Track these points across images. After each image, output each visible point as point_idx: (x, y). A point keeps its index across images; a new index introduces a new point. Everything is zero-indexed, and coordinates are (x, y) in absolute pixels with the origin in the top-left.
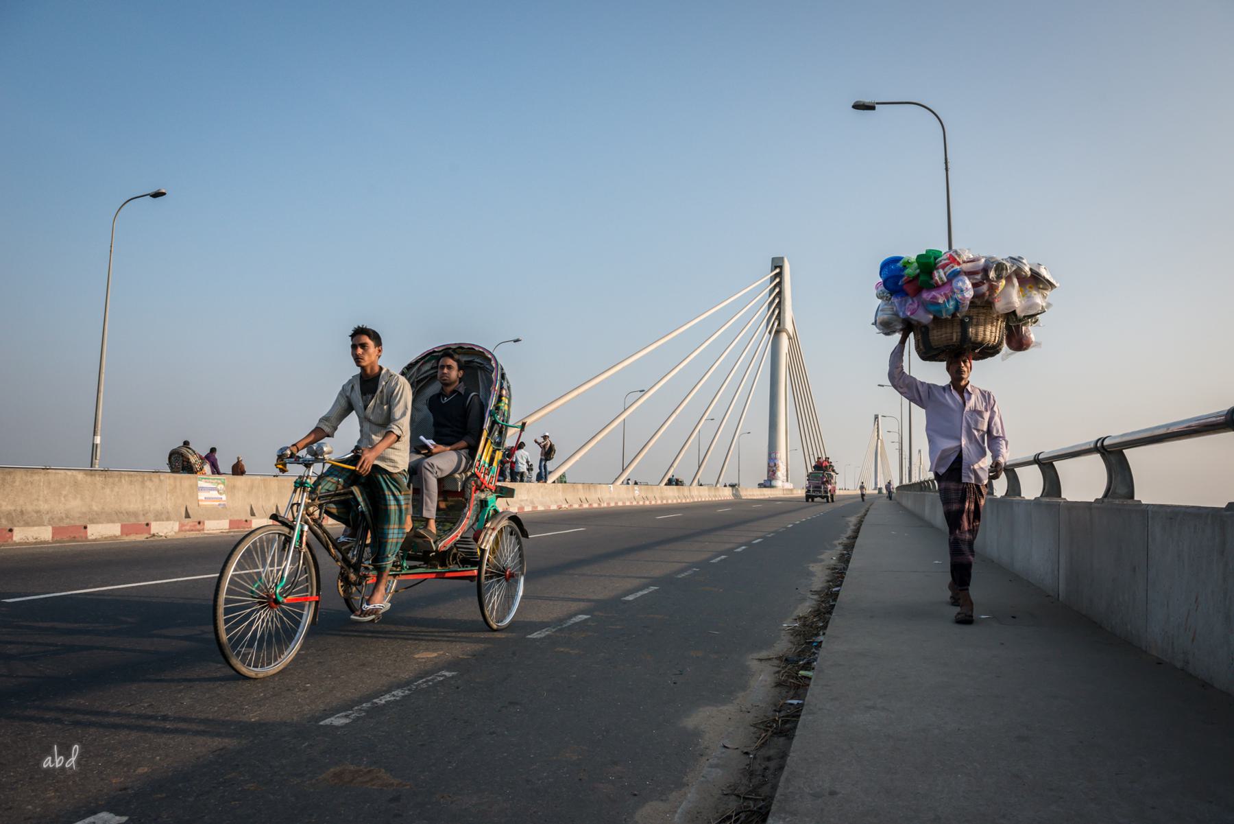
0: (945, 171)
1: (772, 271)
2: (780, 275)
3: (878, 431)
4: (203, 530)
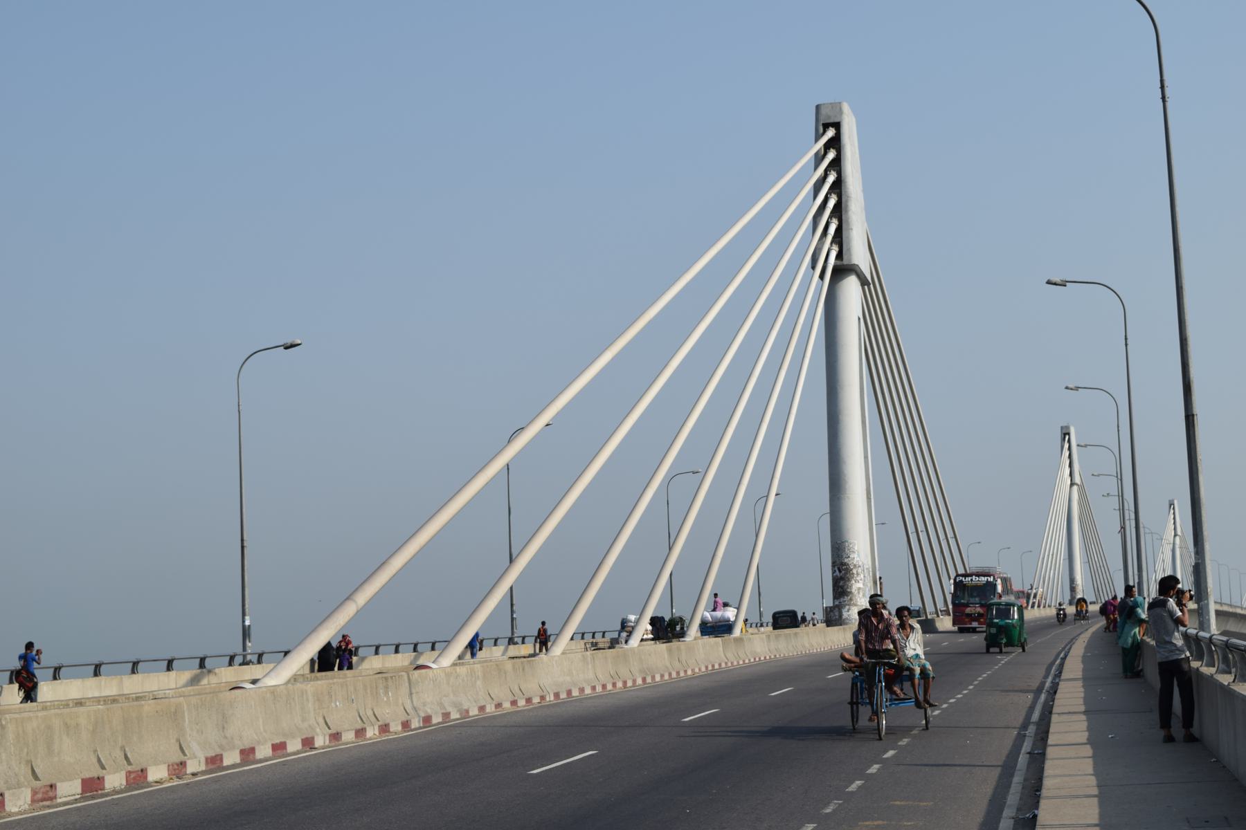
0: (1160, 90)
1: (817, 139)
2: (835, 143)
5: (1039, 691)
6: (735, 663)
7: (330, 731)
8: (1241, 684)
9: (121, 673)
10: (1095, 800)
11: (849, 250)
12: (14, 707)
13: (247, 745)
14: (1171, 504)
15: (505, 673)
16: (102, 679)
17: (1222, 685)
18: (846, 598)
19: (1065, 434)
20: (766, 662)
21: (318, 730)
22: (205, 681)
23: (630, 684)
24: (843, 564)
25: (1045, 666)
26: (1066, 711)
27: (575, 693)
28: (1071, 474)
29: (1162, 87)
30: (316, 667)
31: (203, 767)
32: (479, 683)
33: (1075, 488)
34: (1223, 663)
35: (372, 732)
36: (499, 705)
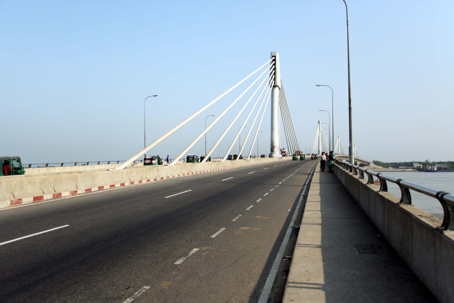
0: (347, 25)
1: (271, 58)
2: (274, 60)
3: (320, 128)
4: (22, 202)
5: (310, 174)
6: (247, 165)
7: (130, 182)
8: (370, 184)
9: (105, 164)
10: (320, 226)
11: (276, 82)
12: (30, 175)
13: (101, 185)
14: (338, 136)
15: (187, 167)
16: (77, 166)
17: (363, 184)
18: (273, 152)
19: (319, 122)
20: (254, 165)
21: (127, 181)
22: (135, 166)
23: (220, 169)
24: (273, 145)
25: (312, 168)
26: (315, 182)
27: (206, 171)
28: (320, 130)
29: (347, 22)
30: (14, 174)
31: (84, 192)
32: (179, 169)
33: (320, 132)
34: (361, 175)
35: (190, 174)
36: (184, 175)
